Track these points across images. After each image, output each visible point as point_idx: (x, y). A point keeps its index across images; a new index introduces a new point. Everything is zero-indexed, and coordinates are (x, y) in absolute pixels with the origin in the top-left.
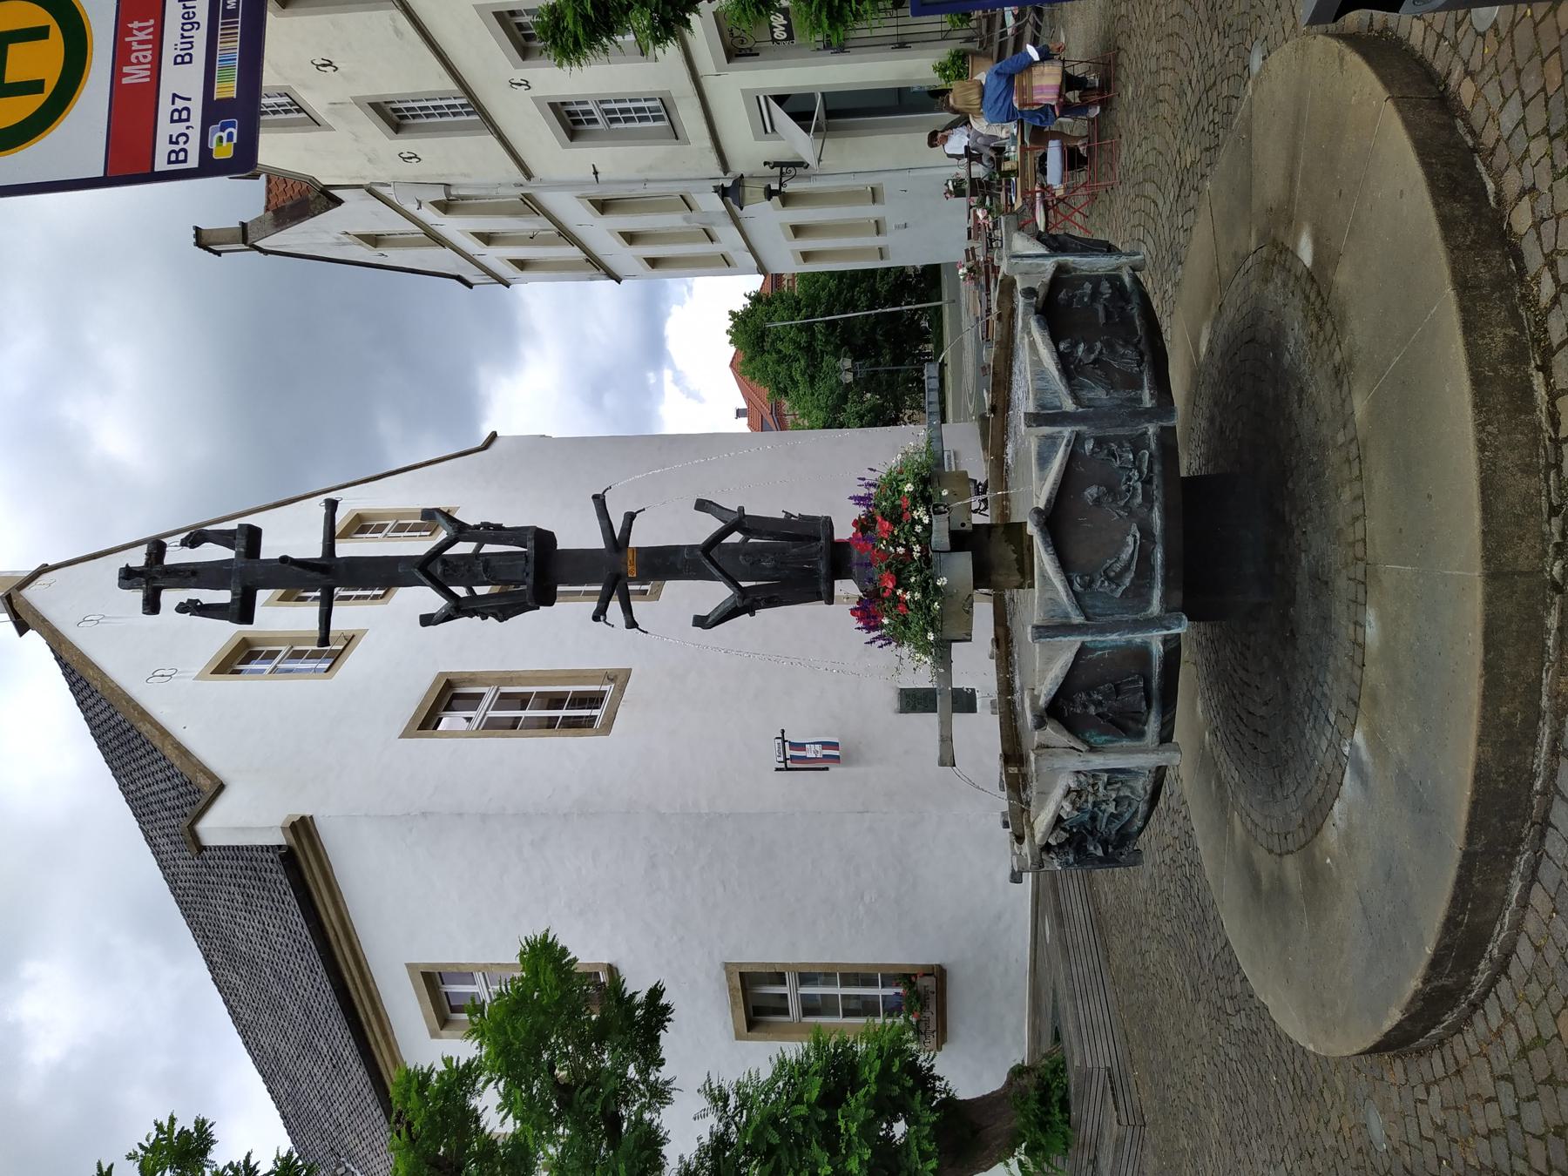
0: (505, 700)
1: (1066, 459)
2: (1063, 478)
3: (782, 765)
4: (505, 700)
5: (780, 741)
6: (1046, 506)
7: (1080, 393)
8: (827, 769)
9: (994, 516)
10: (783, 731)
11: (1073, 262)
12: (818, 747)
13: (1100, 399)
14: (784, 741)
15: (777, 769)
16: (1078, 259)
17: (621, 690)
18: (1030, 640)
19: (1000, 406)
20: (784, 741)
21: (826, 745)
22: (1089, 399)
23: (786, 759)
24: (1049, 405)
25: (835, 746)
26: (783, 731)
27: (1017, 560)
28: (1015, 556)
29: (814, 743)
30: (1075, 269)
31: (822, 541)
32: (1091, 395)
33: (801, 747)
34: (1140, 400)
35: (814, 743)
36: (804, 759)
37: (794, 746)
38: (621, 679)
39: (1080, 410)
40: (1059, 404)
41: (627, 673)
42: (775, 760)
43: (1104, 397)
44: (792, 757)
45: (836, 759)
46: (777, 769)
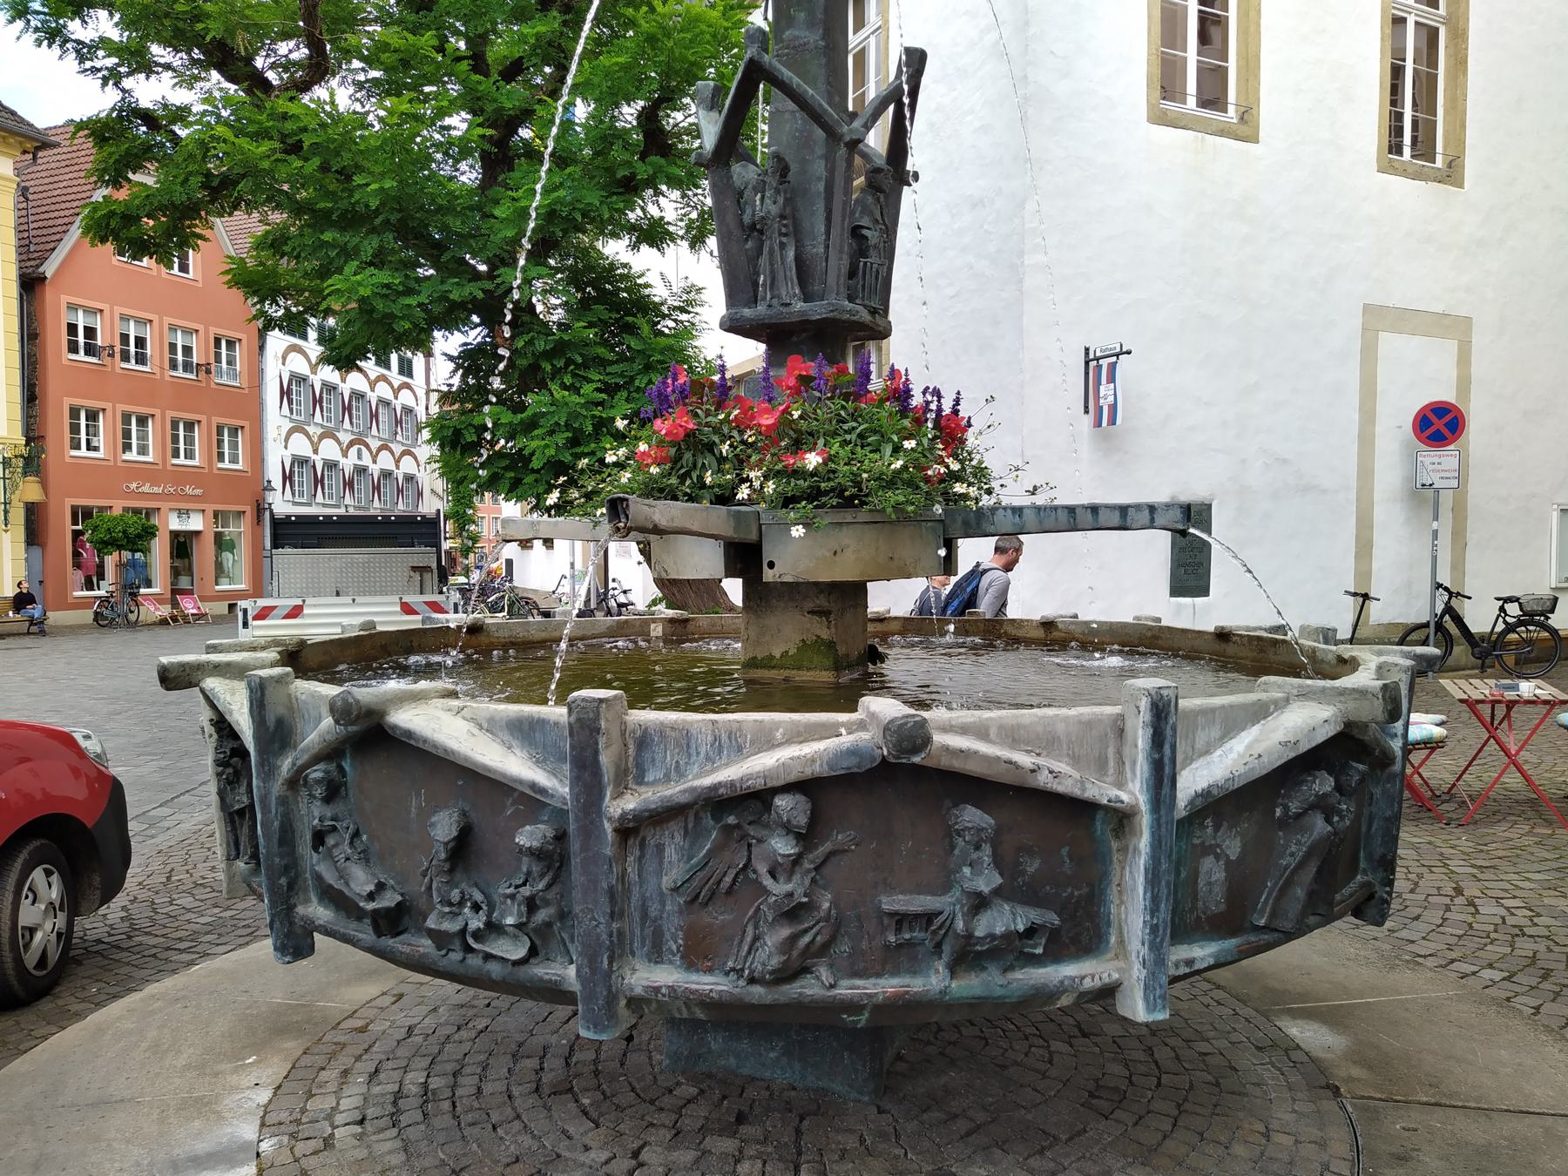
0: (1430, 36)
1: (503, 780)
2: (452, 763)
3: (1091, 356)
4: (1430, 36)
5: (1118, 350)
6: (395, 727)
7: (675, 827)
8: (1086, 411)
9: (1072, 627)
10: (1129, 353)
11: (1136, 850)
12: (1111, 399)
13: (659, 873)
14: (1117, 355)
15: (1087, 350)
16: (1142, 861)
17: (1225, 132)
18: (165, 660)
19: (1230, 649)
20: (1117, 355)
21: (1113, 408)
22: (660, 849)
23: (1097, 359)
24: (647, 756)
25: (1112, 421)
26: (1129, 353)
27: (771, 657)
28: (778, 656)
29: (1115, 395)
30: (1124, 850)
31: (799, 306)
32: (671, 853)
33: (1112, 379)
34: (657, 955)
35: (1115, 395)
36: (1098, 383)
37: (1112, 367)
38: (1244, 131)
39: (608, 827)
40: (650, 777)
41: (1253, 138)
42: (1097, 348)
43: (667, 882)
44: (1099, 367)
45: (1098, 424)
46: (1087, 350)
